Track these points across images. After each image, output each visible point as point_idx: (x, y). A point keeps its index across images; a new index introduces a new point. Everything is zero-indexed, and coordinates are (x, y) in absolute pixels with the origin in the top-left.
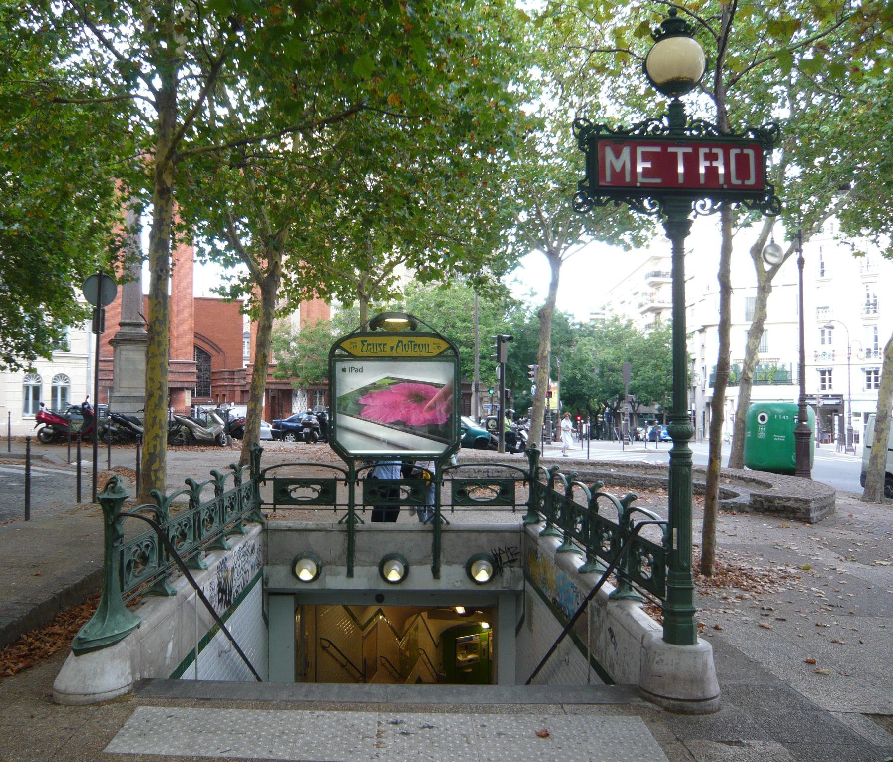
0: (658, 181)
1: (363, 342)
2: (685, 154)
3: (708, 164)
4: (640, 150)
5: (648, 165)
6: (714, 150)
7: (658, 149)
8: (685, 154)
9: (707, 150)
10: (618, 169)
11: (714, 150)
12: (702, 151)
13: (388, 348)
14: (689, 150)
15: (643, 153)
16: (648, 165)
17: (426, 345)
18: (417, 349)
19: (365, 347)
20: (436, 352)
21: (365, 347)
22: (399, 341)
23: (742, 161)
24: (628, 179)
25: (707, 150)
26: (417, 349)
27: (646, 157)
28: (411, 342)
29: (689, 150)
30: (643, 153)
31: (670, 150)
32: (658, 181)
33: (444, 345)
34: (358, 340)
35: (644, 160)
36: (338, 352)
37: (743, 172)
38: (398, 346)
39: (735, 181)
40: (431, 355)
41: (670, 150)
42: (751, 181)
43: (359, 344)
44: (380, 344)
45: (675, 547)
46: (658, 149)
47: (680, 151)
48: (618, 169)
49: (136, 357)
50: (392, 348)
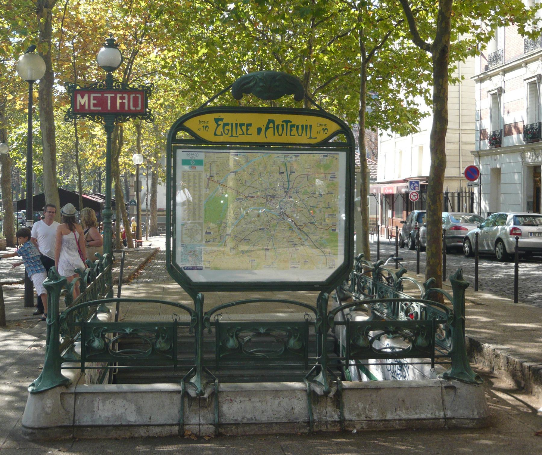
0: (100, 108)
1: (217, 120)
2: (111, 97)
3: (121, 101)
4: (92, 95)
5: (95, 102)
6: (124, 95)
7: (100, 95)
8: (111, 97)
9: (121, 95)
10: (82, 104)
11: (124, 95)
12: (119, 96)
13: (253, 130)
14: (113, 95)
15: (93, 96)
16: (95, 102)
17: (307, 128)
18: (294, 132)
19: (221, 127)
20: (321, 137)
21: (221, 127)
22: (270, 121)
23: (136, 100)
24: (87, 107)
25: (121, 95)
26: (294, 132)
27: (95, 98)
28: (287, 122)
29: (113, 95)
30: (93, 96)
31: (105, 95)
32: (100, 108)
33: (334, 127)
34: (210, 118)
35: (94, 100)
36: (181, 134)
37: (136, 105)
38: (267, 128)
39: (132, 108)
40: (313, 141)
41: (105, 95)
42: (139, 108)
43: (212, 125)
44: (242, 125)
45: (172, 239)
46: (100, 95)
47: (109, 96)
48: (82, 104)
49: (337, 429)
50: (259, 130)
